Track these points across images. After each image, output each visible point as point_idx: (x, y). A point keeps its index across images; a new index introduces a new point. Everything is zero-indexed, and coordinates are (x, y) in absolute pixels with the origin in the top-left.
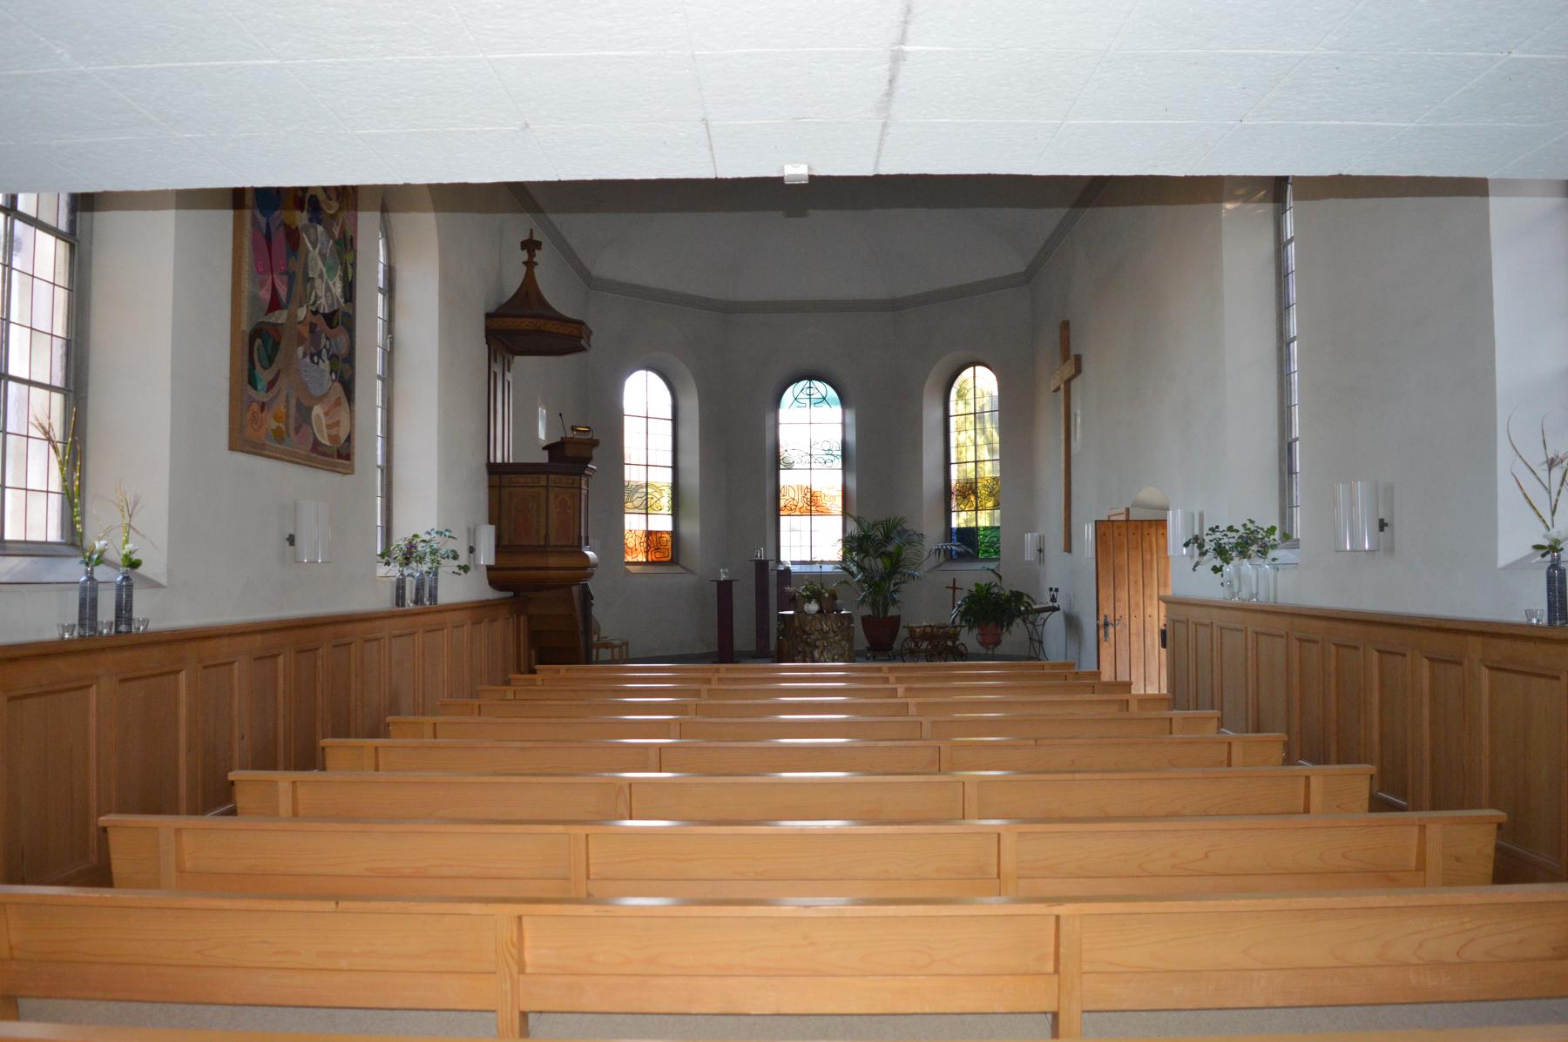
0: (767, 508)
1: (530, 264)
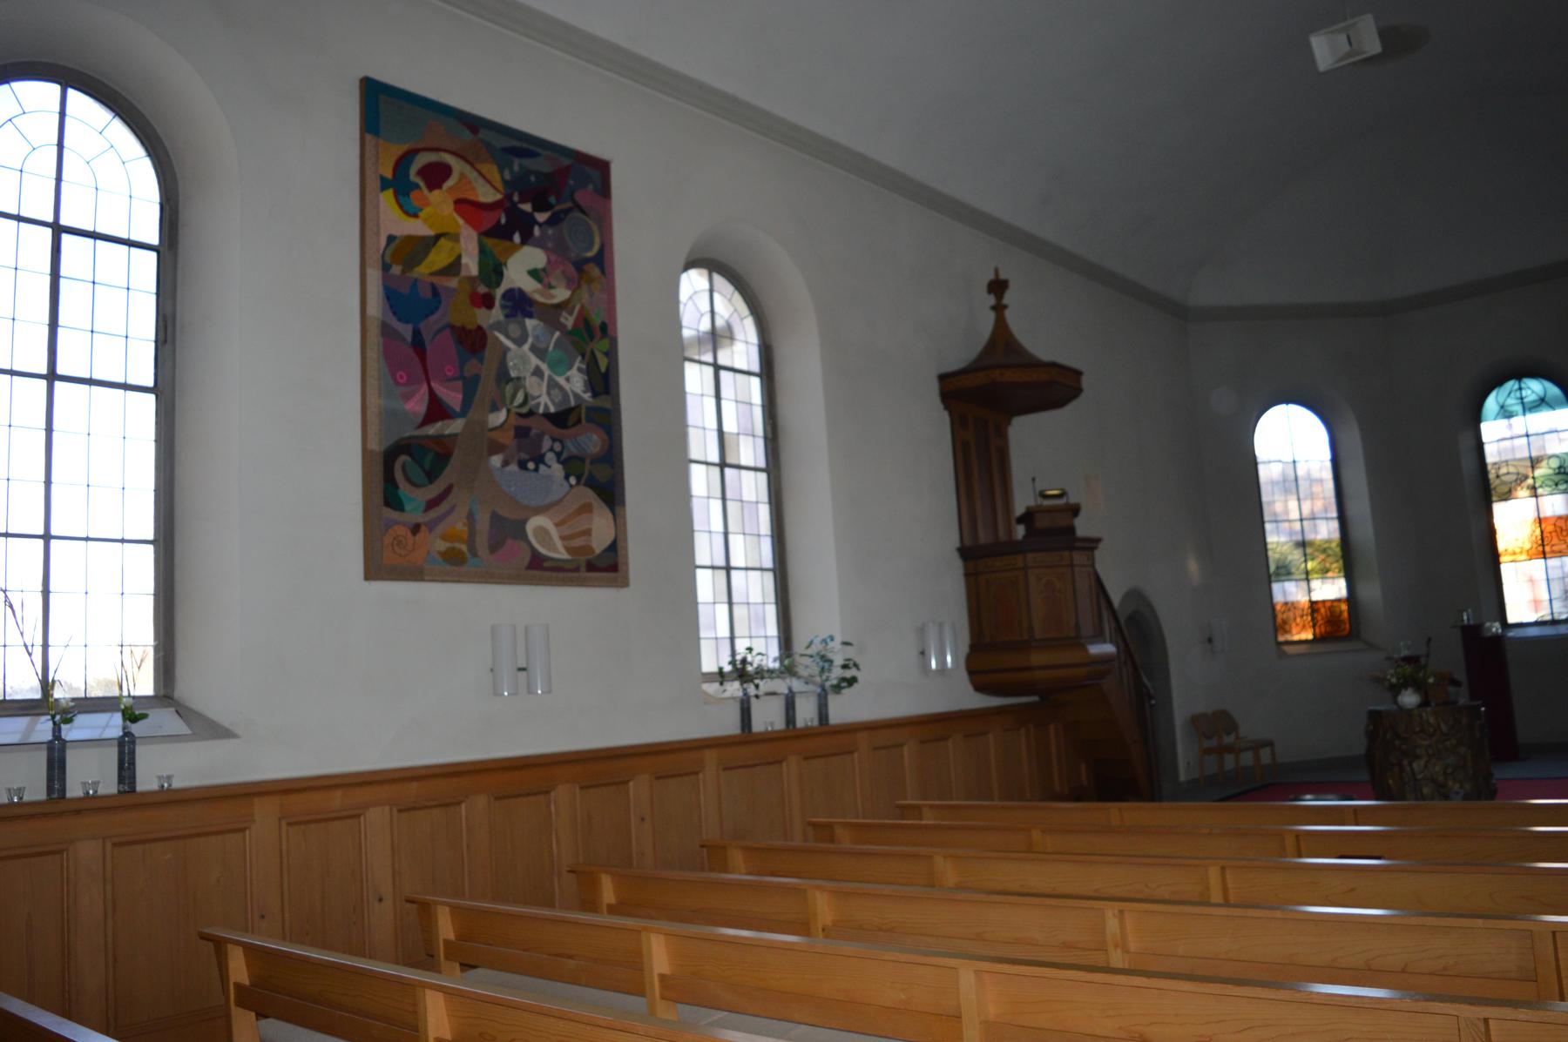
0: (1260, 571)
1: (999, 308)
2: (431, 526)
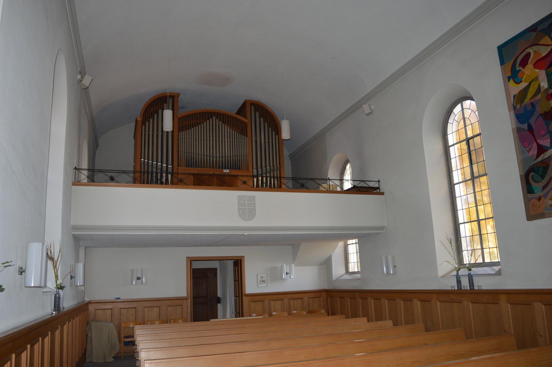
2: (545, 196)
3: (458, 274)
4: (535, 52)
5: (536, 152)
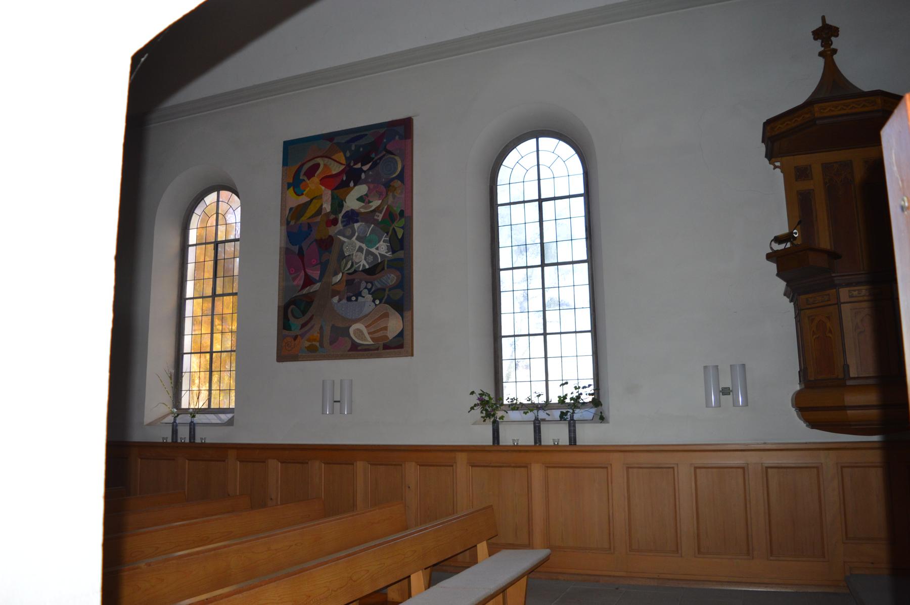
2: (302, 336)
3: (175, 422)
4: (325, 165)
5: (302, 282)
